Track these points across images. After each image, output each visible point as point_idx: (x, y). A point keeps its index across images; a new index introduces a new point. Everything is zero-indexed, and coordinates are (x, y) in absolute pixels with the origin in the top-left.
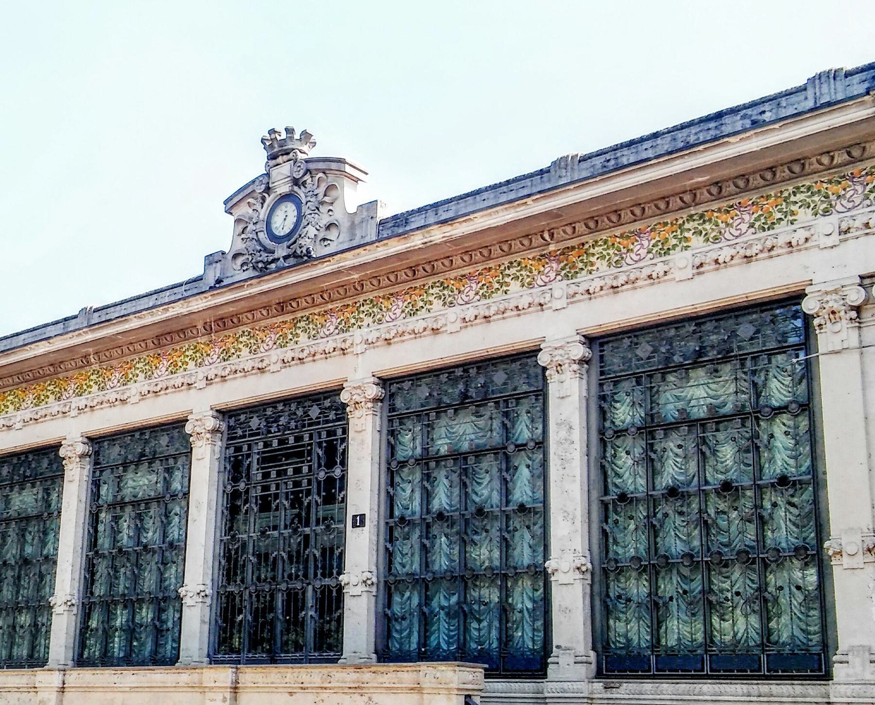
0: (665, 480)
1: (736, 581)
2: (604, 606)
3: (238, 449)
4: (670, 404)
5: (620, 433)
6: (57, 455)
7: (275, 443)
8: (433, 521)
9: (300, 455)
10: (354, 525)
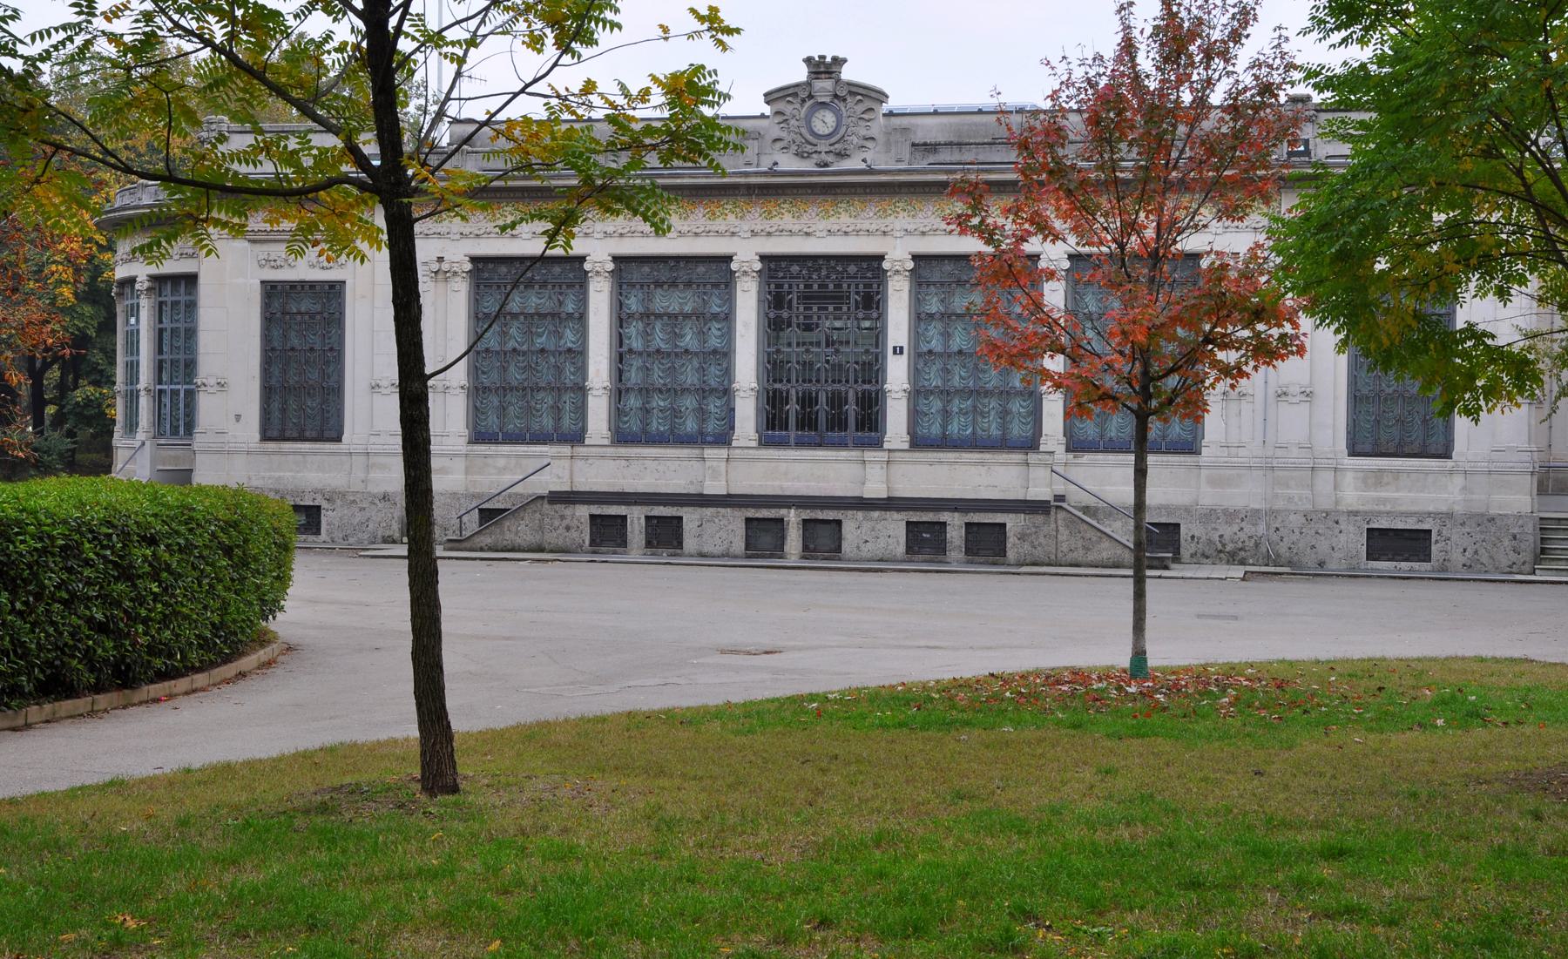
0: (511, 344)
1: (689, 402)
2: (914, 415)
3: (779, 286)
4: (514, 305)
5: (631, 316)
6: (880, 268)
7: (815, 287)
8: (507, 355)
9: (806, 298)
10: (895, 352)
